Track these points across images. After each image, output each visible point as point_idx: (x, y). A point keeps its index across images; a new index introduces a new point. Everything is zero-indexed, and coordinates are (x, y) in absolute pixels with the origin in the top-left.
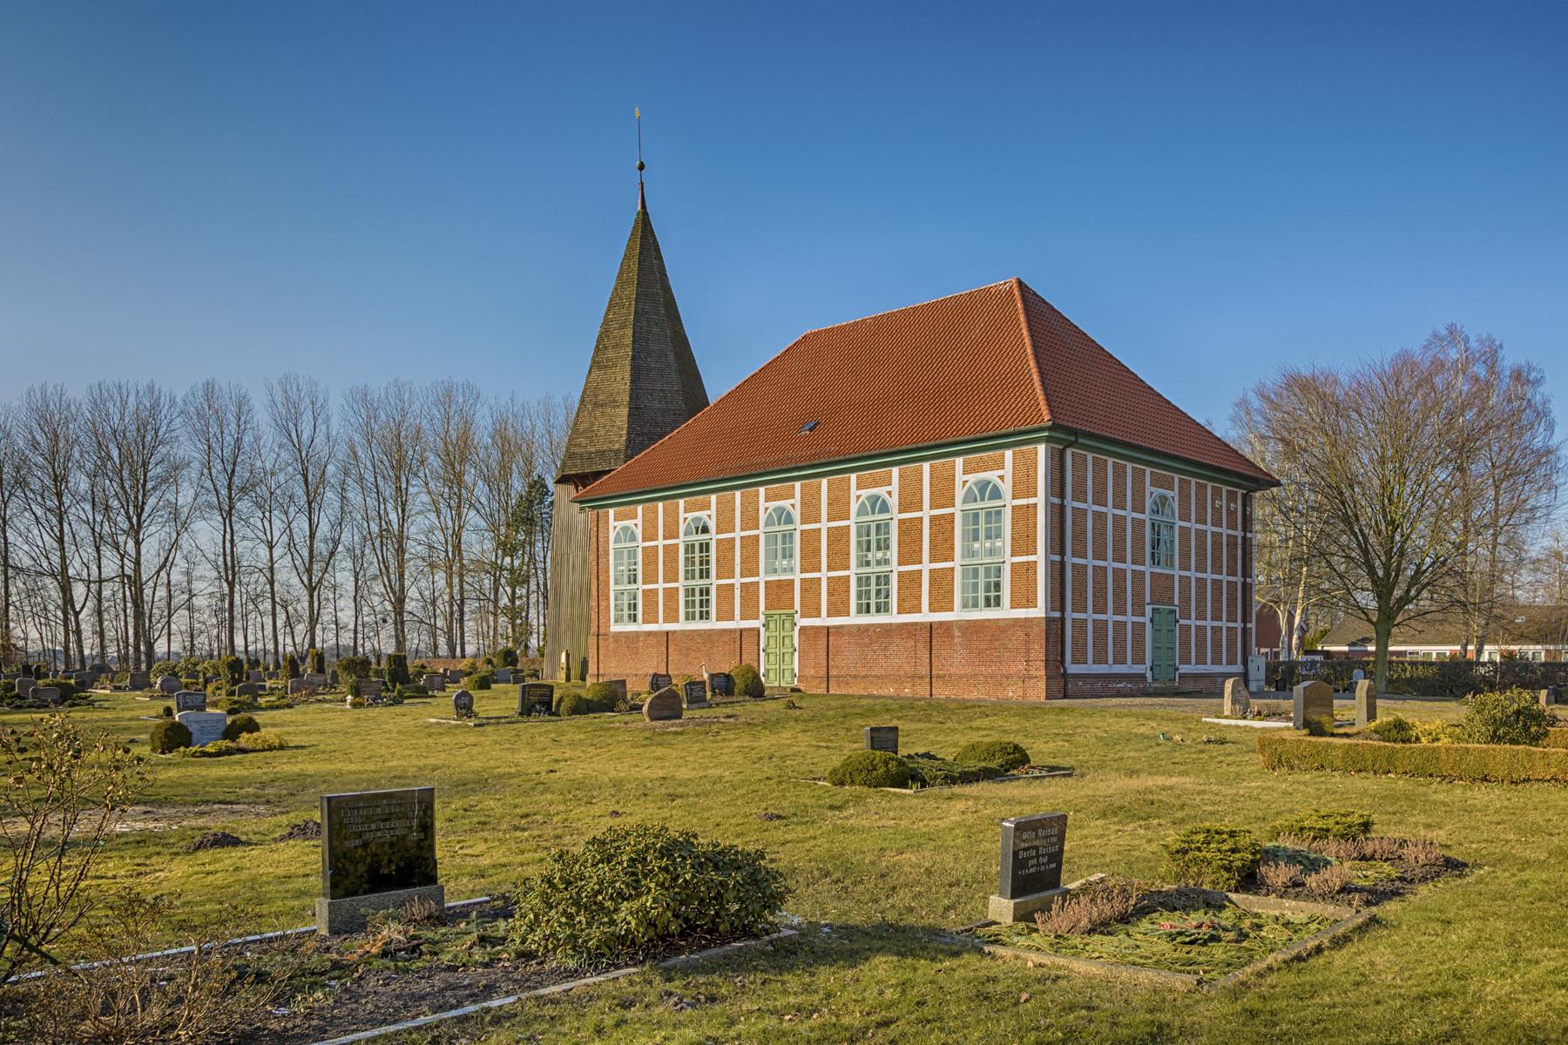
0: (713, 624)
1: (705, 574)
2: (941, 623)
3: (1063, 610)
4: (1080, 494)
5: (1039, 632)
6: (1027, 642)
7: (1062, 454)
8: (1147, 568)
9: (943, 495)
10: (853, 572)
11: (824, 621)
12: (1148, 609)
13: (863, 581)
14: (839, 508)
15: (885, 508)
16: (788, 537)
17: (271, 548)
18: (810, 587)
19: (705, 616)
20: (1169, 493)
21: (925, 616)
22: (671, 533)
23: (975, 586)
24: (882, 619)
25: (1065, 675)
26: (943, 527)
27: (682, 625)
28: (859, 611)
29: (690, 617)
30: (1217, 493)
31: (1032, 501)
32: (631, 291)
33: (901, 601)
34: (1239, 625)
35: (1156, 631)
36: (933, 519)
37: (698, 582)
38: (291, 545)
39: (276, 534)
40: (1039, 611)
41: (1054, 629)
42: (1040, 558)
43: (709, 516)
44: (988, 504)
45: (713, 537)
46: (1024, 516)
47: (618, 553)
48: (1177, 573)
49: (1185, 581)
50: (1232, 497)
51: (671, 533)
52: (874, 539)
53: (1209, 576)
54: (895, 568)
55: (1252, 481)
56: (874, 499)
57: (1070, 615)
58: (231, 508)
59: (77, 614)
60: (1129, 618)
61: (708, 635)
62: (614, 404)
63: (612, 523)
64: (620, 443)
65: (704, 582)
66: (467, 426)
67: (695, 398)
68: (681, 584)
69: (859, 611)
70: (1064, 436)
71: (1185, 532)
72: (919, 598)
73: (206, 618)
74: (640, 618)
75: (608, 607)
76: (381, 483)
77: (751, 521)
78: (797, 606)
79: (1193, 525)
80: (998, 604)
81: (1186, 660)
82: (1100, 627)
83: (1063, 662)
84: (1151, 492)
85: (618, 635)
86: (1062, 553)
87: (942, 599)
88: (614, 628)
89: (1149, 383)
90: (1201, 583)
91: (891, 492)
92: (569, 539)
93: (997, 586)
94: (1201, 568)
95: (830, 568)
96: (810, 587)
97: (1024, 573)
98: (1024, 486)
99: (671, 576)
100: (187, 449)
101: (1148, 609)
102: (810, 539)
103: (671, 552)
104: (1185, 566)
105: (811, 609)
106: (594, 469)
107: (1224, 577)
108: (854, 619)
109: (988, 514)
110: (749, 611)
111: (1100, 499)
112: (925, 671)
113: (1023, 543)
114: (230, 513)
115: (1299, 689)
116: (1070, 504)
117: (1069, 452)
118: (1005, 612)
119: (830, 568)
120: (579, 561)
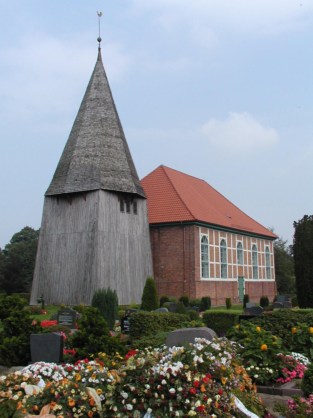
85: (204, 282)
88: (202, 279)
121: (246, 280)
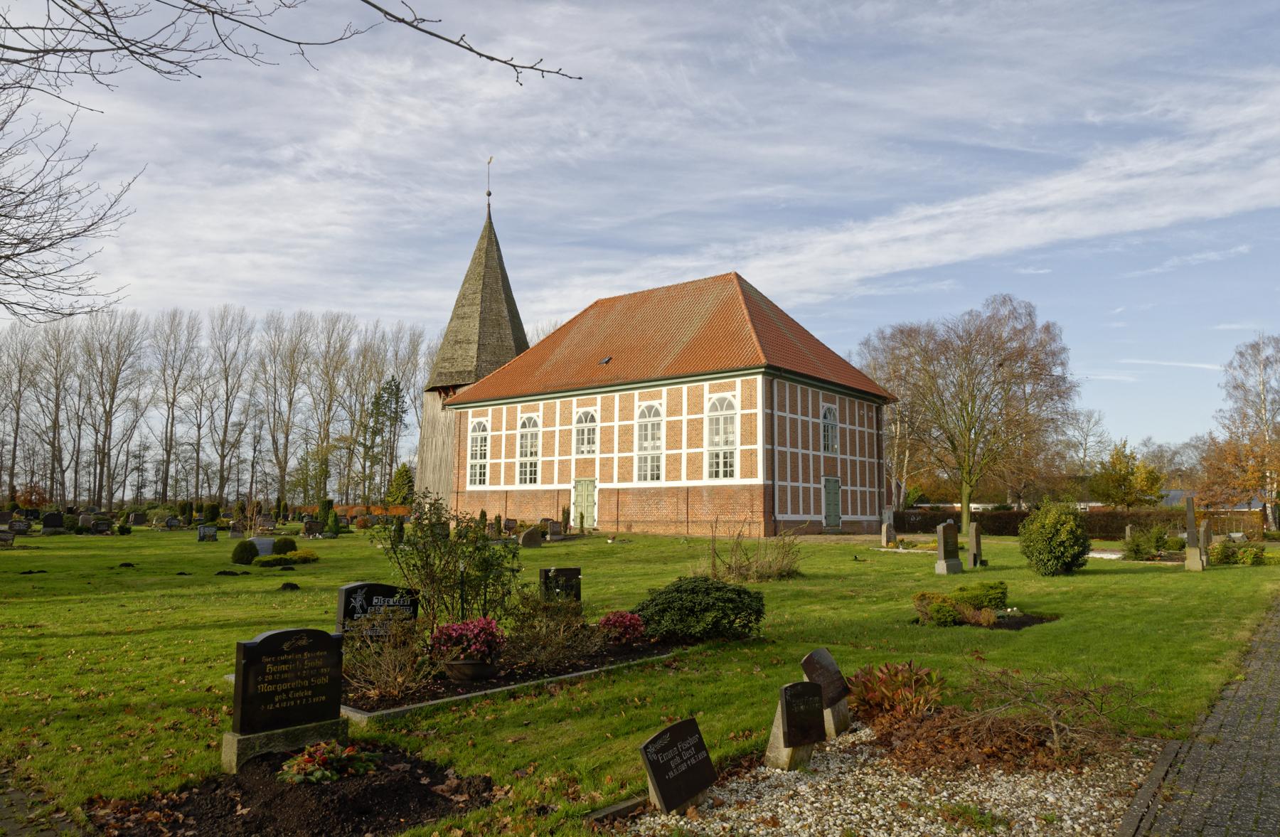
0: (538, 486)
1: (484, 456)
2: (695, 488)
3: (773, 480)
4: (782, 408)
5: (760, 492)
8: (822, 454)
9: (696, 406)
10: (636, 454)
11: (616, 485)
12: (823, 479)
13: (643, 460)
14: (626, 413)
17: (199, 427)
18: (606, 463)
20: (833, 406)
21: (684, 482)
22: (511, 426)
23: (718, 464)
24: (655, 484)
25: (775, 521)
26: (695, 426)
27: (517, 486)
28: (640, 479)
29: (523, 481)
30: (861, 407)
31: (753, 411)
33: (668, 472)
35: (828, 493)
36: (689, 422)
37: (529, 459)
38: (213, 429)
39: (204, 419)
40: (759, 480)
42: (759, 446)
44: (725, 412)
46: (748, 420)
47: (474, 440)
48: (839, 456)
49: (844, 462)
51: (511, 426)
52: (649, 432)
53: (858, 458)
58: (174, 400)
59: (63, 472)
61: (535, 494)
63: (470, 419)
64: (471, 365)
65: (483, 461)
66: (343, 347)
68: (518, 460)
69: (640, 479)
71: (843, 431)
72: (679, 471)
73: (150, 475)
74: (487, 481)
75: (465, 475)
76: (278, 384)
77: (566, 419)
79: (848, 426)
83: (773, 513)
84: (823, 406)
85: (472, 492)
86: (773, 444)
87: (695, 472)
88: (469, 488)
89: (817, 334)
91: (661, 404)
92: (434, 428)
93: (658, 467)
95: (620, 451)
96: (606, 463)
97: (749, 456)
98: (748, 402)
99: (510, 454)
100: (151, 361)
101: (823, 479)
102: (607, 432)
103: (510, 439)
106: (454, 383)
109: (725, 419)
110: (564, 477)
112: (683, 517)
113: (748, 437)
114: (173, 404)
115: (940, 528)
116: (777, 413)
117: (775, 382)
118: (737, 480)
119: (620, 451)
120: (440, 443)
121: (599, 485)
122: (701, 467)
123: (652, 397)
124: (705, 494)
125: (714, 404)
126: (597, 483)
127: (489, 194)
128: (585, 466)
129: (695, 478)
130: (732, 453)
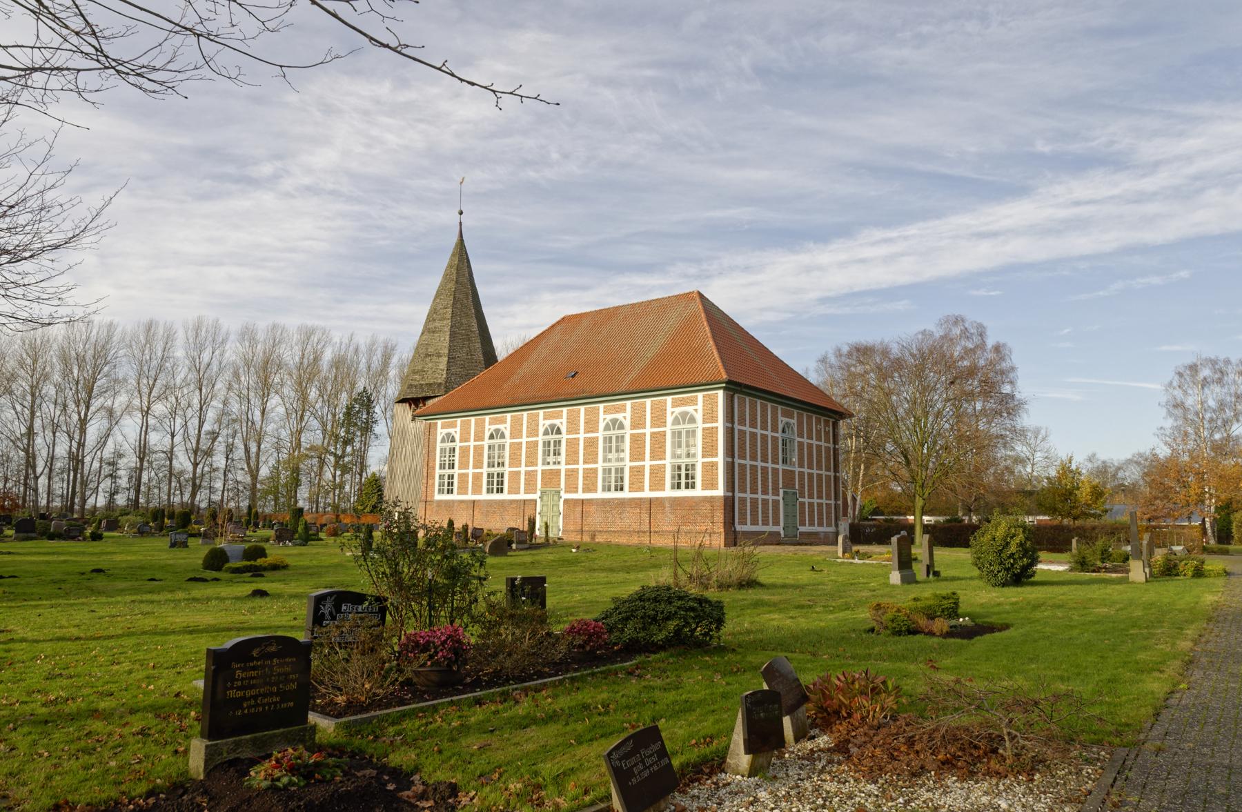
1: (452, 466)
4: (742, 422)
5: (720, 504)
6: (712, 511)
7: (732, 397)
8: (780, 467)
9: (659, 419)
11: (580, 495)
12: (781, 492)
13: (607, 471)
15: (621, 427)
16: (621, 439)
17: (173, 436)
18: (571, 474)
19: (500, 491)
20: (792, 421)
21: (647, 494)
22: (479, 437)
23: (679, 476)
24: (619, 495)
26: (658, 439)
27: (484, 496)
28: (604, 490)
29: (490, 491)
30: (818, 421)
32: (452, 285)
33: (631, 484)
34: (832, 502)
35: (786, 505)
36: (653, 434)
38: (186, 437)
39: (177, 428)
40: (720, 491)
41: (729, 503)
43: (456, 432)
44: (617, 432)
45: (458, 444)
46: (710, 434)
47: (443, 450)
48: (797, 469)
49: (801, 474)
50: (827, 423)
52: (613, 444)
53: (815, 472)
54: (628, 464)
55: (832, 414)
56: (448, 435)
57: (737, 495)
59: (37, 478)
60: (770, 497)
61: (501, 503)
62: (439, 355)
64: (441, 377)
67: (489, 356)
69: (604, 490)
70: (733, 388)
71: (801, 444)
72: (642, 482)
78: (563, 485)
80: (693, 487)
81: (803, 524)
82: (754, 502)
83: (733, 524)
84: (782, 421)
88: (438, 497)
90: (811, 475)
91: (626, 417)
92: (403, 438)
93: (622, 479)
94: (810, 466)
95: (585, 462)
96: (571, 474)
97: (710, 468)
98: (710, 416)
99: (478, 465)
101: (781, 492)
102: (572, 444)
104: (801, 466)
105: (572, 488)
106: (424, 395)
107: (823, 472)
108: (600, 495)
109: (688, 432)
110: (530, 487)
111: (753, 425)
112: (646, 528)
113: (709, 450)
114: (147, 412)
115: (894, 539)
116: (737, 427)
119: (585, 462)
121: (564, 496)
122: (664, 479)
123: (618, 410)
124: (667, 505)
125: (607, 425)
126: (562, 493)
127: (461, 213)
128: (551, 477)
129: (657, 490)
130: (693, 465)
